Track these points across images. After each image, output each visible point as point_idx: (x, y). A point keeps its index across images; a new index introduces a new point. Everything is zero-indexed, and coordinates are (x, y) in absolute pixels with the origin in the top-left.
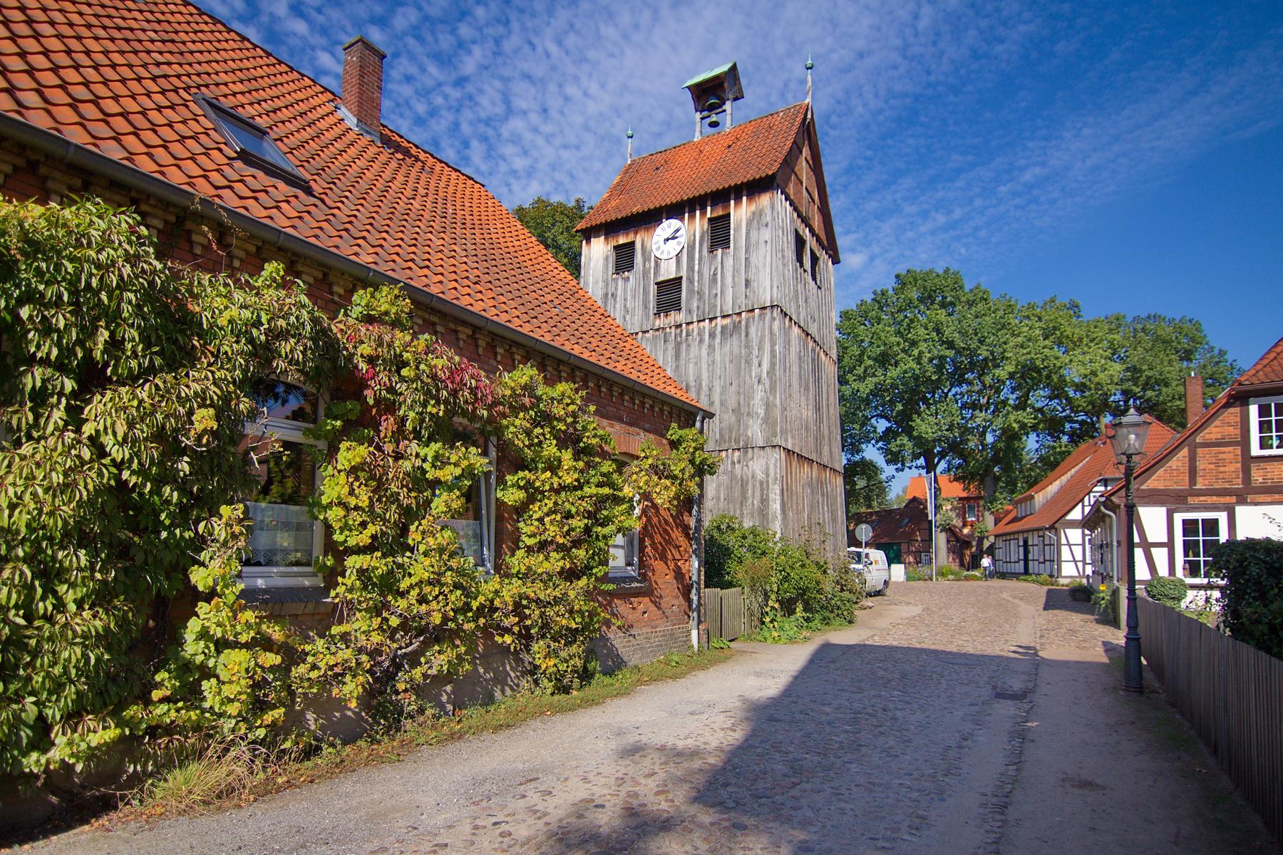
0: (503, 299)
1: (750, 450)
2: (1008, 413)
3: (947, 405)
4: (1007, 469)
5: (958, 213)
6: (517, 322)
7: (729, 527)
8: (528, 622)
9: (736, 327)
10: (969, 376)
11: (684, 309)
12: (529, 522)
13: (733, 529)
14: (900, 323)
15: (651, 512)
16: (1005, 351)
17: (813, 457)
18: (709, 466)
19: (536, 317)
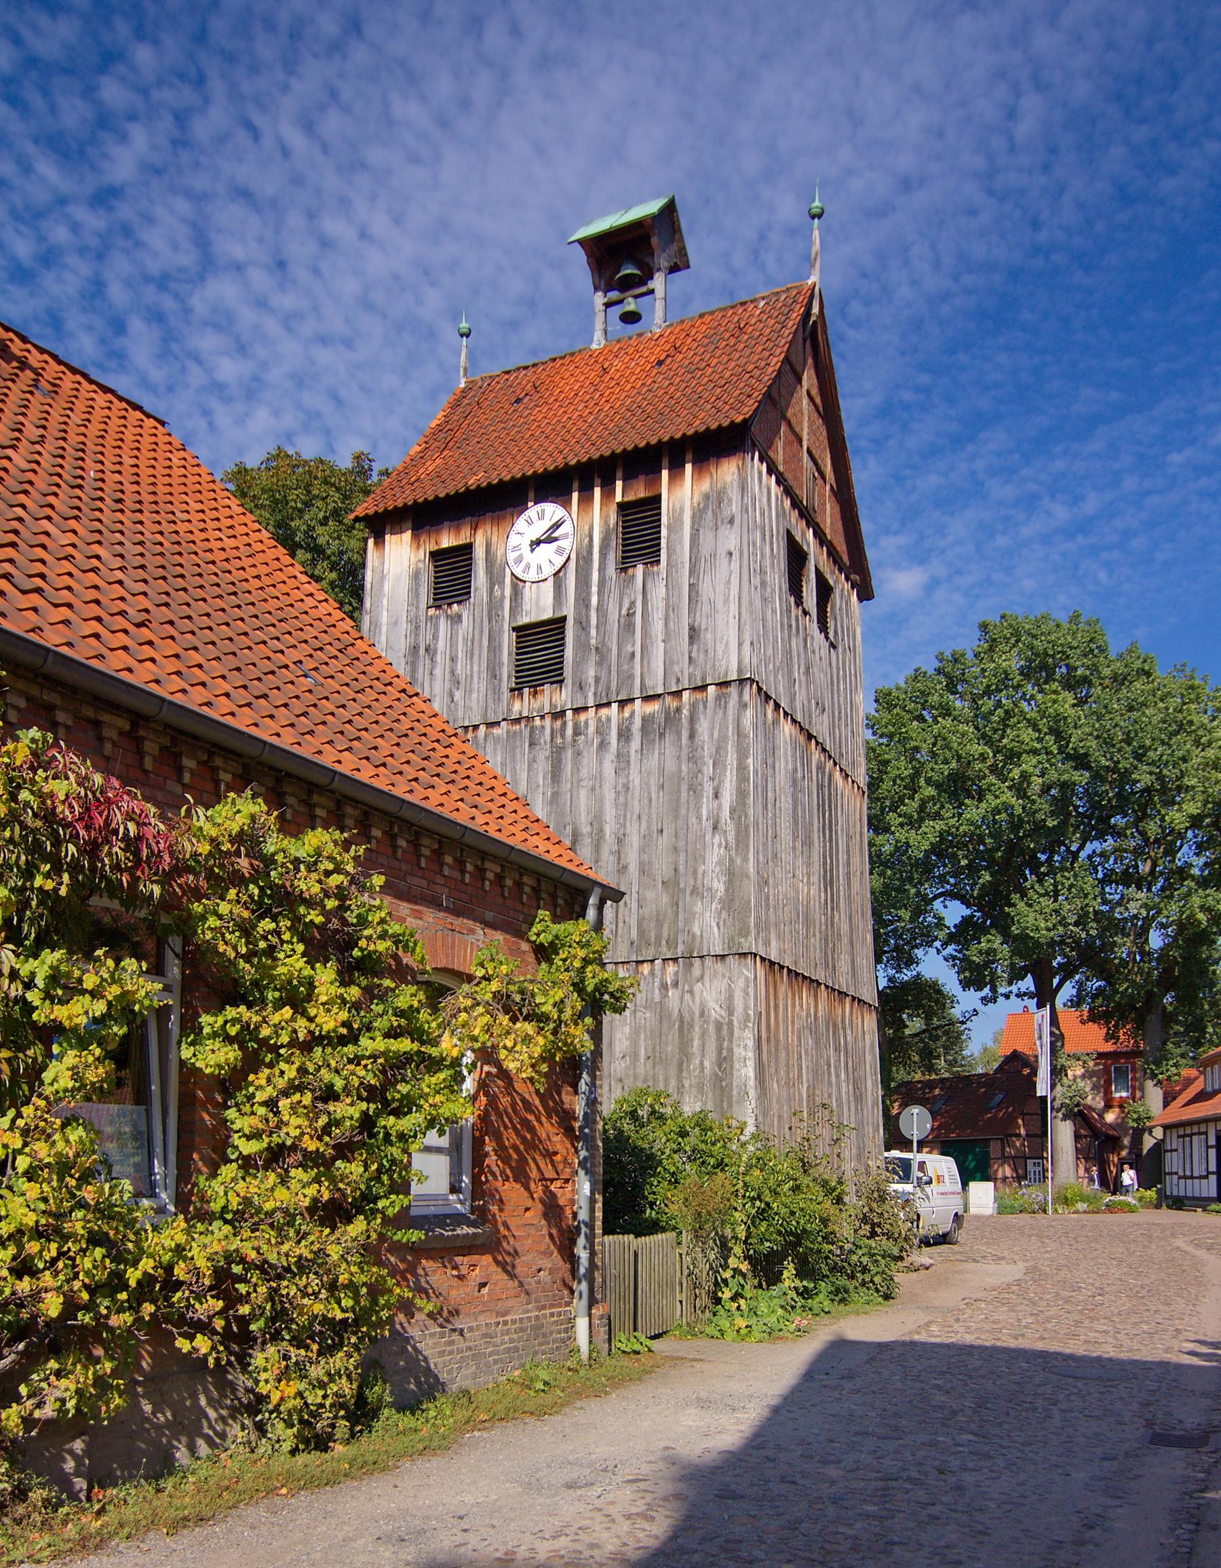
0: (196, 658)
1: (697, 962)
2: (1189, 894)
3: (1075, 876)
4: (1188, 999)
5: (1092, 504)
6: (224, 705)
7: (653, 1112)
8: (244, 1310)
9: (671, 718)
10: (1118, 820)
11: (569, 681)
12: (247, 1109)
13: (662, 1118)
14: (986, 717)
15: (497, 1087)
16: (1183, 775)
17: (819, 975)
18: (612, 995)
19: (265, 696)
